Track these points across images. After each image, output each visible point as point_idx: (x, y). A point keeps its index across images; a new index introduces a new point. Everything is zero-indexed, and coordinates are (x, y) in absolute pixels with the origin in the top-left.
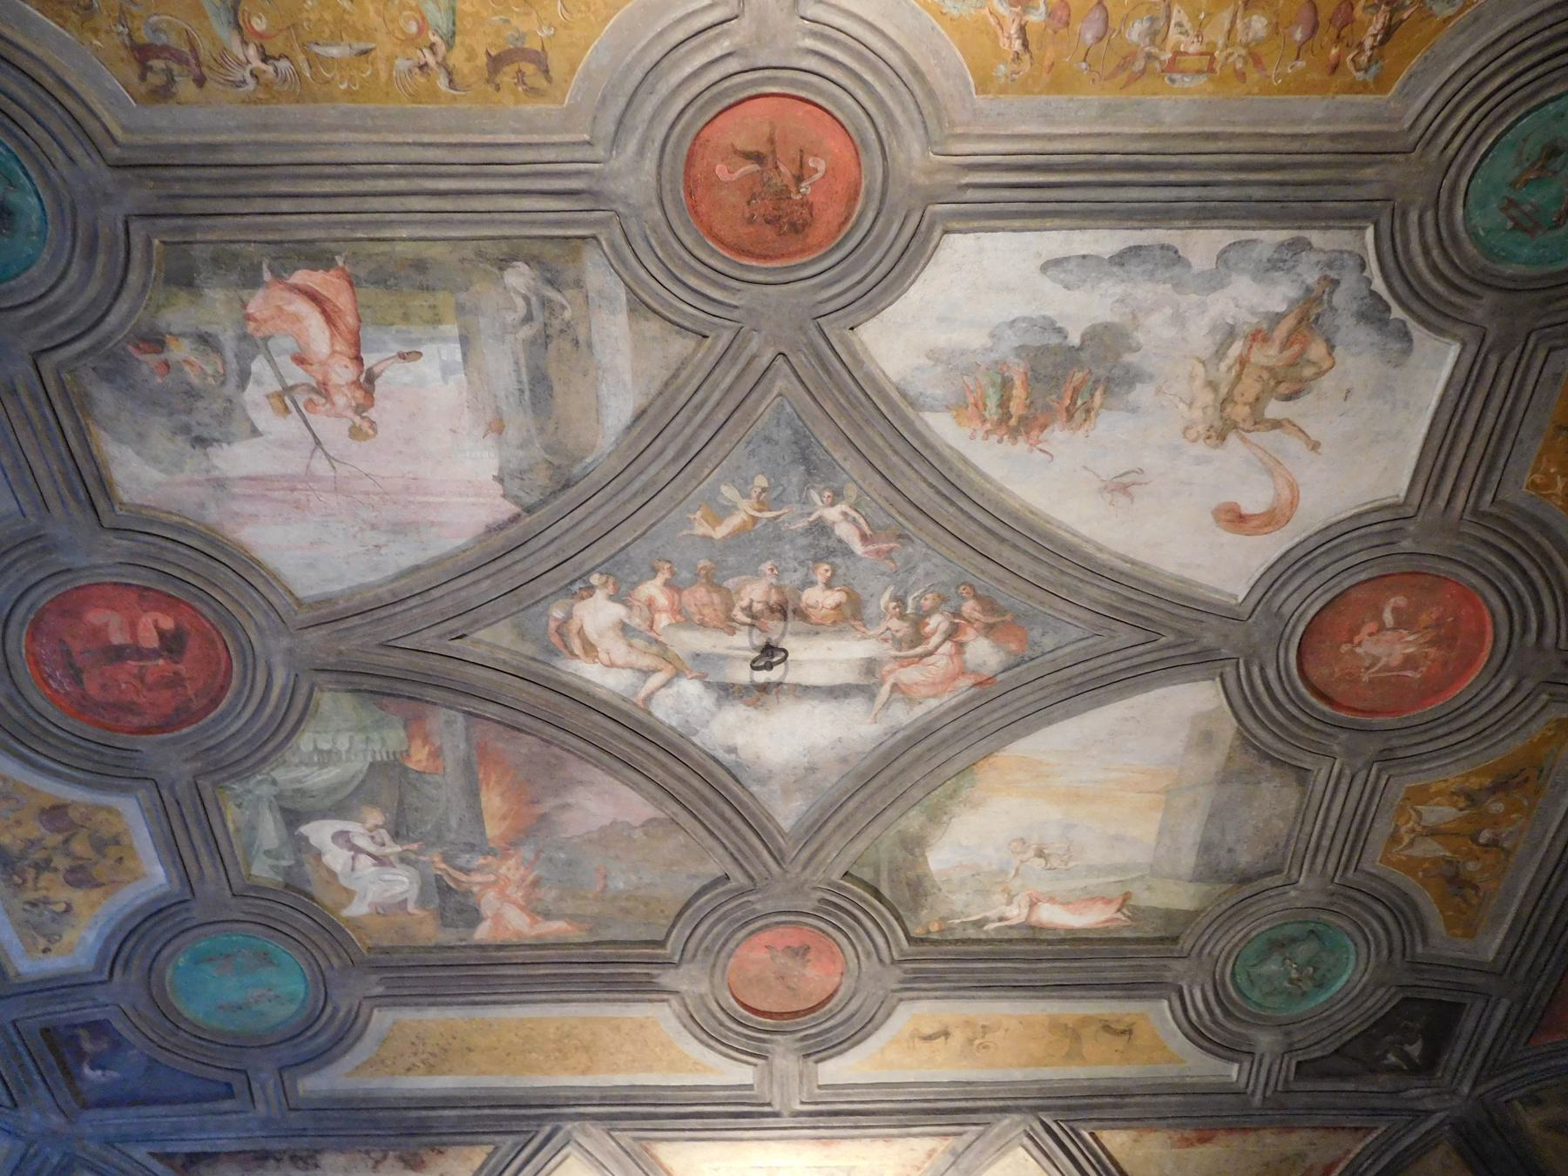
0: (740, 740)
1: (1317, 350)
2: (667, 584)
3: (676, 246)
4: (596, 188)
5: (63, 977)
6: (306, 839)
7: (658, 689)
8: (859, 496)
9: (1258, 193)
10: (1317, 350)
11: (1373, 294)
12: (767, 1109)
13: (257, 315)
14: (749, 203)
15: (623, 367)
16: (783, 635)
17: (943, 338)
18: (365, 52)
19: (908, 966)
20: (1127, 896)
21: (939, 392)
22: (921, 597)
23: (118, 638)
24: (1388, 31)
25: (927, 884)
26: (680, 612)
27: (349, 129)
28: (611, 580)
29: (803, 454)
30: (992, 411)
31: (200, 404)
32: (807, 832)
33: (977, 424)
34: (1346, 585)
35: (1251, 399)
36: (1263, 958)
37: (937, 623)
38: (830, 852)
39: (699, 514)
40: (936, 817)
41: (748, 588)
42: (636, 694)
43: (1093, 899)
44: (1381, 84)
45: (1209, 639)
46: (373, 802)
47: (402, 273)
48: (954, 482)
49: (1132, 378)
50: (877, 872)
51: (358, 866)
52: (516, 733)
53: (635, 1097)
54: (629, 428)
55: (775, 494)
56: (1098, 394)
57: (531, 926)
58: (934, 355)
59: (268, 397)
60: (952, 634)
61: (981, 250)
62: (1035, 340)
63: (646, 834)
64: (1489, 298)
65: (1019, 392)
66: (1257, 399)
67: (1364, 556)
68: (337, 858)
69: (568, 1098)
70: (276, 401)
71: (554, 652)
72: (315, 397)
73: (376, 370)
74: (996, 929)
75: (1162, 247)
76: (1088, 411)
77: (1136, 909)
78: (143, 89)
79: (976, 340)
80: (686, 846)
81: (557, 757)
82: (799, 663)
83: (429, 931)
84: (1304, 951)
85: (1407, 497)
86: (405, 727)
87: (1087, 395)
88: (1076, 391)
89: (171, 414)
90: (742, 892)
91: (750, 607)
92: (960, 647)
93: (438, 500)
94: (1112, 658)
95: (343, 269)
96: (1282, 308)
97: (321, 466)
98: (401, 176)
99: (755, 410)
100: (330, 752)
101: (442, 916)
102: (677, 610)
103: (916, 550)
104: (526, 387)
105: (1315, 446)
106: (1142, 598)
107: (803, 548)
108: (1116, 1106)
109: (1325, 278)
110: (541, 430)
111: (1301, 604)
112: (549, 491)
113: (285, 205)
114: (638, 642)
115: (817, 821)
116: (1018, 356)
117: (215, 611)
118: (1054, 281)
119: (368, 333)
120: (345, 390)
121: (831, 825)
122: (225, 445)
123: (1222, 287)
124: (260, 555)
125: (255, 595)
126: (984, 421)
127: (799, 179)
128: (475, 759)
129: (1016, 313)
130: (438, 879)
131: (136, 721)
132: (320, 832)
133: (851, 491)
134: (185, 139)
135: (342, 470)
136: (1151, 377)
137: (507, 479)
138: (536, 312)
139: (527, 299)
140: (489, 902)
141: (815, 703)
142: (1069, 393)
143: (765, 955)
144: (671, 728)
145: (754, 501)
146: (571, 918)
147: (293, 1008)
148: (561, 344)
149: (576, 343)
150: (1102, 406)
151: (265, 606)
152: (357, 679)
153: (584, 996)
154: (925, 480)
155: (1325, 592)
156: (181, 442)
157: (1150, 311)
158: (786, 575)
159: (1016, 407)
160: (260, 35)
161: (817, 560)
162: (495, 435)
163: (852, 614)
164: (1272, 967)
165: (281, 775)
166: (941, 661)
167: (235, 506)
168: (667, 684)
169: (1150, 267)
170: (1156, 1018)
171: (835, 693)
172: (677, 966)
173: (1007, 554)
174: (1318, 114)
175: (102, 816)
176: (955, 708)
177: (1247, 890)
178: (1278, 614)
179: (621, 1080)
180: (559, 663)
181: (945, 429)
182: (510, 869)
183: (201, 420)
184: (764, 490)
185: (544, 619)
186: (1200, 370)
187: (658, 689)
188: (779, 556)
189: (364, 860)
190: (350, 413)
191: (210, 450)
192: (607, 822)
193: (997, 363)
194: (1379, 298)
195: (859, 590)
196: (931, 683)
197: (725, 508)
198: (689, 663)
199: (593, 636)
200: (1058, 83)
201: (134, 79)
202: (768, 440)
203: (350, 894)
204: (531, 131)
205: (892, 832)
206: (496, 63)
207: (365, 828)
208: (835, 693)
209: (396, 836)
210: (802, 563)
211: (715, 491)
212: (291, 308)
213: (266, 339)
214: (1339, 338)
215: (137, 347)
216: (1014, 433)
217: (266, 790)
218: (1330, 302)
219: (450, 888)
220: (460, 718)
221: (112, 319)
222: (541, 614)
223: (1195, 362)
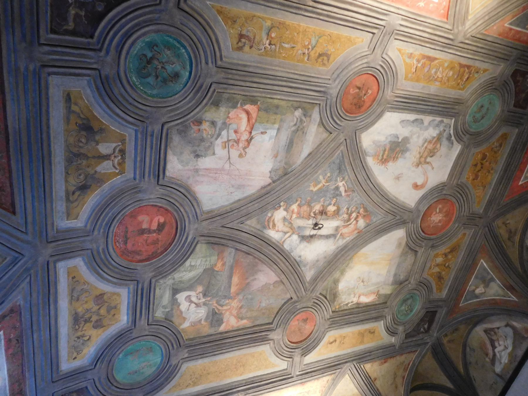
0: (302, 253)
1: (438, 146)
2: (298, 205)
4: (326, 91)
5: (79, 369)
6: (177, 299)
9: (440, 109)
10: (438, 146)
11: (450, 134)
12: (290, 376)
13: (231, 117)
18: (293, 47)
19: (331, 320)
21: (372, 152)
23: (145, 226)
24: (468, 78)
25: (337, 294)
26: (299, 214)
27: (280, 67)
30: (380, 158)
31: (203, 144)
36: (402, 305)
37: (354, 215)
40: (343, 273)
43: (372, 293)
44: (462, 89)
45: (405, 217)
49: (407, 150)
50: (327, 291)
51: (190, 308)
53: (256, 380)
57: (237, 323)
58: (374, 142)
64: (468, 136)
65: (386, 153)
68: (184, 306)
69: (235, 385)
70: (224, 144)
71: (265, 228)
72: (235, 144)
78: (236, 46)
83: (206, 330)
84: (409, 302)
92: (357, 221)
97: (227, 166)
98: (286, 81)
100: (193, 266)
101: (211, 324)
103: (356, 194)
104: (287, 144)
105: (433, 168)
108: (370, 356)
110: (286, 157)
113: (255, 85)
119: (257, 125)
120: (243, 142)
127: (365, 95)
129: (392, 133)
130: (213, 309)
131: (139, 258)
133: (347, 178)
134: (240, 62)
135: (232, 167)
139: (297, 119)
143: (297, 323)
144: (287, 251)
147: (154, 369)
148: (300, 133)
149: (303, 132)
153: (248, 346)
156: (192, 156)
159: (385, 157)
160: (272, 38)
161: (333, 198)
164: (403, 308)
167: (198, 178)
168: (290, 236)
170: (380, 326)
172: (275, 330)
174: (453, 93)
175: (115, 297)
179: (251, 375)
180: (265, 231)
182: (235, 304)
189: (193, 305)
190: (241, 150)
191: (199, 159)
192: (264, 283)
196: (349, 233)
198: (296, 230)
199: (276, 222)
200: (418, 80)
201: (235, 42)
202: (334, 163)
203: (185, 319)
204: (318, 74)
206: (320, 55)
208: (327, 237)
209: (205, 295)
211: (318, 177)
212: (240, 116)
213: (230, 124)
216: (383, 163)
219: (216, 313)
220: (234, 251)
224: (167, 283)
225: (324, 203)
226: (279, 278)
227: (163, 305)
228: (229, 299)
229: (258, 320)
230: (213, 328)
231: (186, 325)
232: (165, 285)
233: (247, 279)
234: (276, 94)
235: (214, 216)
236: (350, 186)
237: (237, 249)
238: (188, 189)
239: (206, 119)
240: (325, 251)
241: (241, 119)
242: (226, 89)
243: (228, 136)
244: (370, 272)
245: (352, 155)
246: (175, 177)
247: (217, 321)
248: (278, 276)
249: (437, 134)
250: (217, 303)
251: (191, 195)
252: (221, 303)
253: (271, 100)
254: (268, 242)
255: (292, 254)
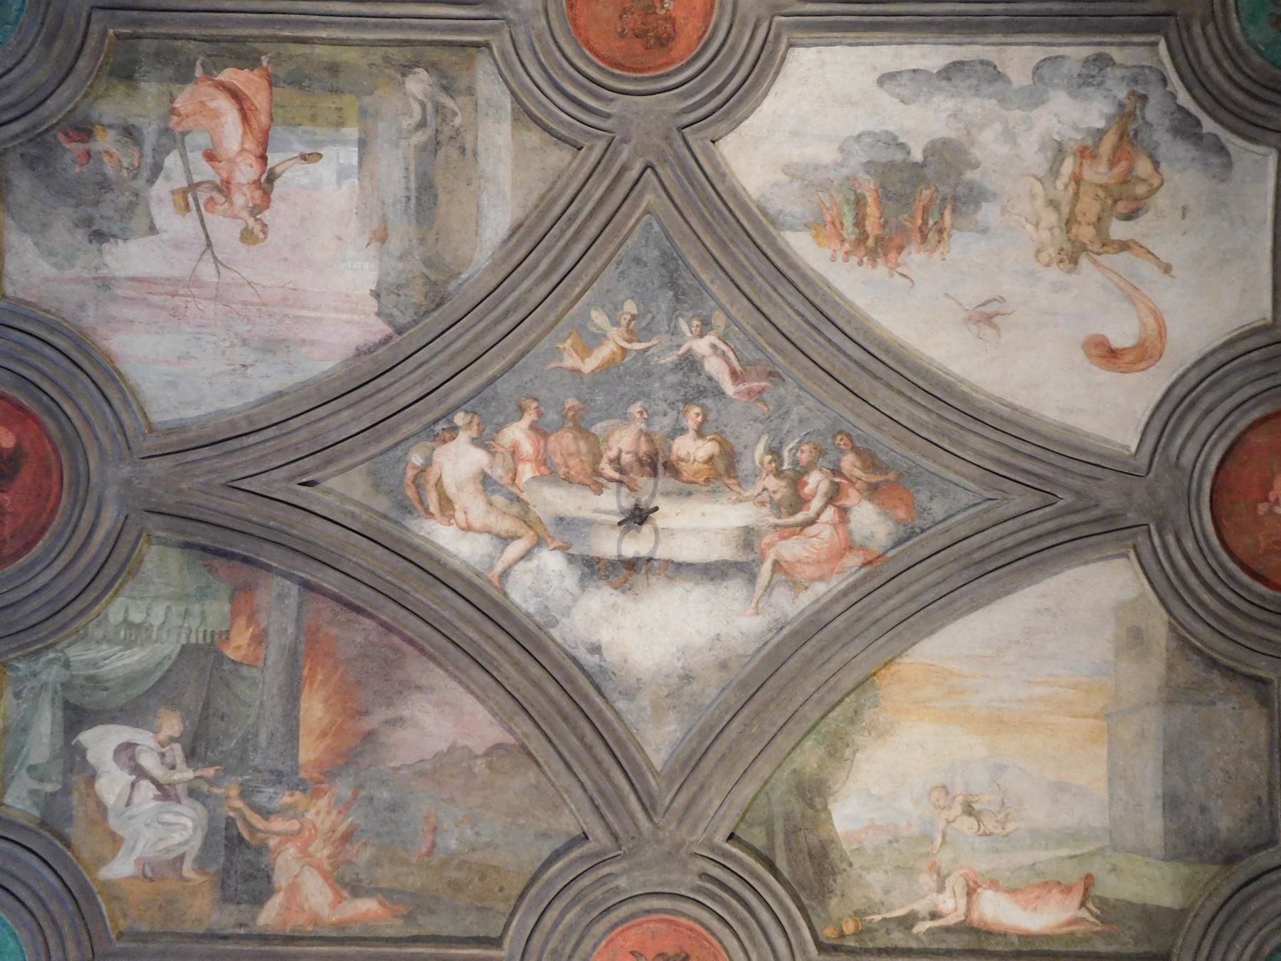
0: (604, 636)
1: (1143, 167)
2: (533, 427)
3: (558, 54)
6: (82, 751)
7: (516, 561)
8: (727, 326)
11: (1181, 108)
13: (182, 111)
14: (621, 17)
15: (507, 171)
16: (653, 495)
17: (795, 153)
20: (1089, 881)
21: (797, 210)
22: (797, 448)
25: (834, 855)
26: (545, 464)
28: (476, 420)
29: (671, 277)
30: (850, 231)
31: (109, 196)
32: (683, 767)
33: (836, 244)
34: (1242, 425)
35: (1094, 219)
37: (816, 482)
38: (711, 800)
39: (569, 341)
40: (837, 750)
41: (617, 435)
42: (491, 567)
45: (1111, 501)
46: (173, 704)
47: (316, 75)
48: (823, 311)
50: (770, 834)
51: (136, 800)
52: (353, 615)
54: (505, 242)
55: (644, 323)
56: (947, 213)
57: (333, 906)
58: (791, 170)
59: (173, 193)
60: (834, 496)
61: (823, 64)
62: (885, 156)
63: (490, 766)
65: (872, 210)
66: (1099, 219)
67: (1249, 391)
68: (112, 783)
70: (179, 198)
71: (406, 509)
72: (216, 195)
73: (278, 170)
74: (930, 932)
75: (982, 62)
76: (940, 231)
77: (1102, 902)
79: (828, 154)
80: (536, 787)
81: (396, 650)
82: (671, 532)
83: (204, 910)
85: (1274, 318)
86: (232, 599)
87: (936, 216)
88: (926, 210)
89: (78, 206)
90: (601, 860)
91: (618, 458)
92: (844, 512)
93: (314, 314)
94: (1010, 526)
95: (266, 69)
96: (1101, 124)
97: (207, 271)
99: (625, 224)
100: (139, 626)
101: (223, 885)
102: (542, 460)
103: (788, 390)
104: (413, 194)
105: (1167, 269)
106: (1028, 449)
107: (672, 387)
109: (1133, 93)
110: (422, 241)
111: (1200, 452)
112: (423, 309)
114: (499, 500)
115: (694, 751)
116: (868, 173)
117: (62, 430)
118: (891, 95)
119: (278, 132)
121: (712, 756)
122: (120, 241)
123: (1043, 103)
124: (124, 367)
125: (107, 409)
126: (843, 241)
128: (302, 647)
129: (861, 128)
132: (101, 743)
133: (719, 320)
135: (227, 276)
136: (995, 195)
137: (383, 294)
138: (430, 119)
140: (286, 864)
141: (689, 585)
142: (920, 212)
144: (529, 616)
145: (623, 329)
146: (387, 895)
149: (463, 150)
150: (953, 226)
151: (115, 427)
152: (191, 526)
154: (792, 307)
155: (1222, 436)
156: (81, 235)
157: (982, 127)
158: (656, 419)
159: (871, 226)
161: (687, 402)
162: (378, 244)
163: (725, 470)
165: (77, 653)
166: (824, 532)
167: (114, 310)
169: (975, 82)
171: (712, 572)
173: (882, 396)
176: (845, 593)
177: (1242, 872)
178: (1177, 465)
181: (804, 247)
182: (320, 814)
183: (103, 214)
184: (634, 317)
185: (402, 466)
186: (1038, 188)
187: (516, 561)
188: (648, 396)
189: (146, 788)
190: (245, 214)
191: (106, 246)
192: (444, 746)
193: (848, 178)
194: (1189, 114)
195: (732, 441)
197: (595, 336)
198: (551, 530)
199: (451, 490)
202: (637, 260)
205: (785, 773)
207: (156, 741)
208: (712, 572)
209: (192, 755)
210: (672, 405)
212: (214, 104)
213: (184, 134)
214: (1161, 152)
215: (66, 135)
216: (873, 254)
217: (53, 675)
218: (1143, 118)
219: (241, 839)
220: (294, 589)
221: (51, 103)
222: (399, 460)
223: (1034, 180)
224: (44, 677)
225: (648, 422)
226: (511, 731)
227: (31, 761)
228: (294, 788)
229: (432, 912)
230: (232, 907)
231: (120, 869)
232: (34, 683)
233: (364, 713)
234: (313, 25)
235: (190, 445)
236: (751, 354)
237: (305, 585)
238: (82, 341)
239: (106, 120)
240: (718, 637)
241: (216, 114)
242: (141, 23)
243: (188, 173)
244: (1001, 768)
245: (708, 226)
246: (34, 300)
247: (248, 878)
248: (502, 722)
249: (1109, 119)
250: (243, 795)
251: (96, 363)
252: (261, 799)
253: (306, 49)
254: (434, 570)
255: (555, 633)
